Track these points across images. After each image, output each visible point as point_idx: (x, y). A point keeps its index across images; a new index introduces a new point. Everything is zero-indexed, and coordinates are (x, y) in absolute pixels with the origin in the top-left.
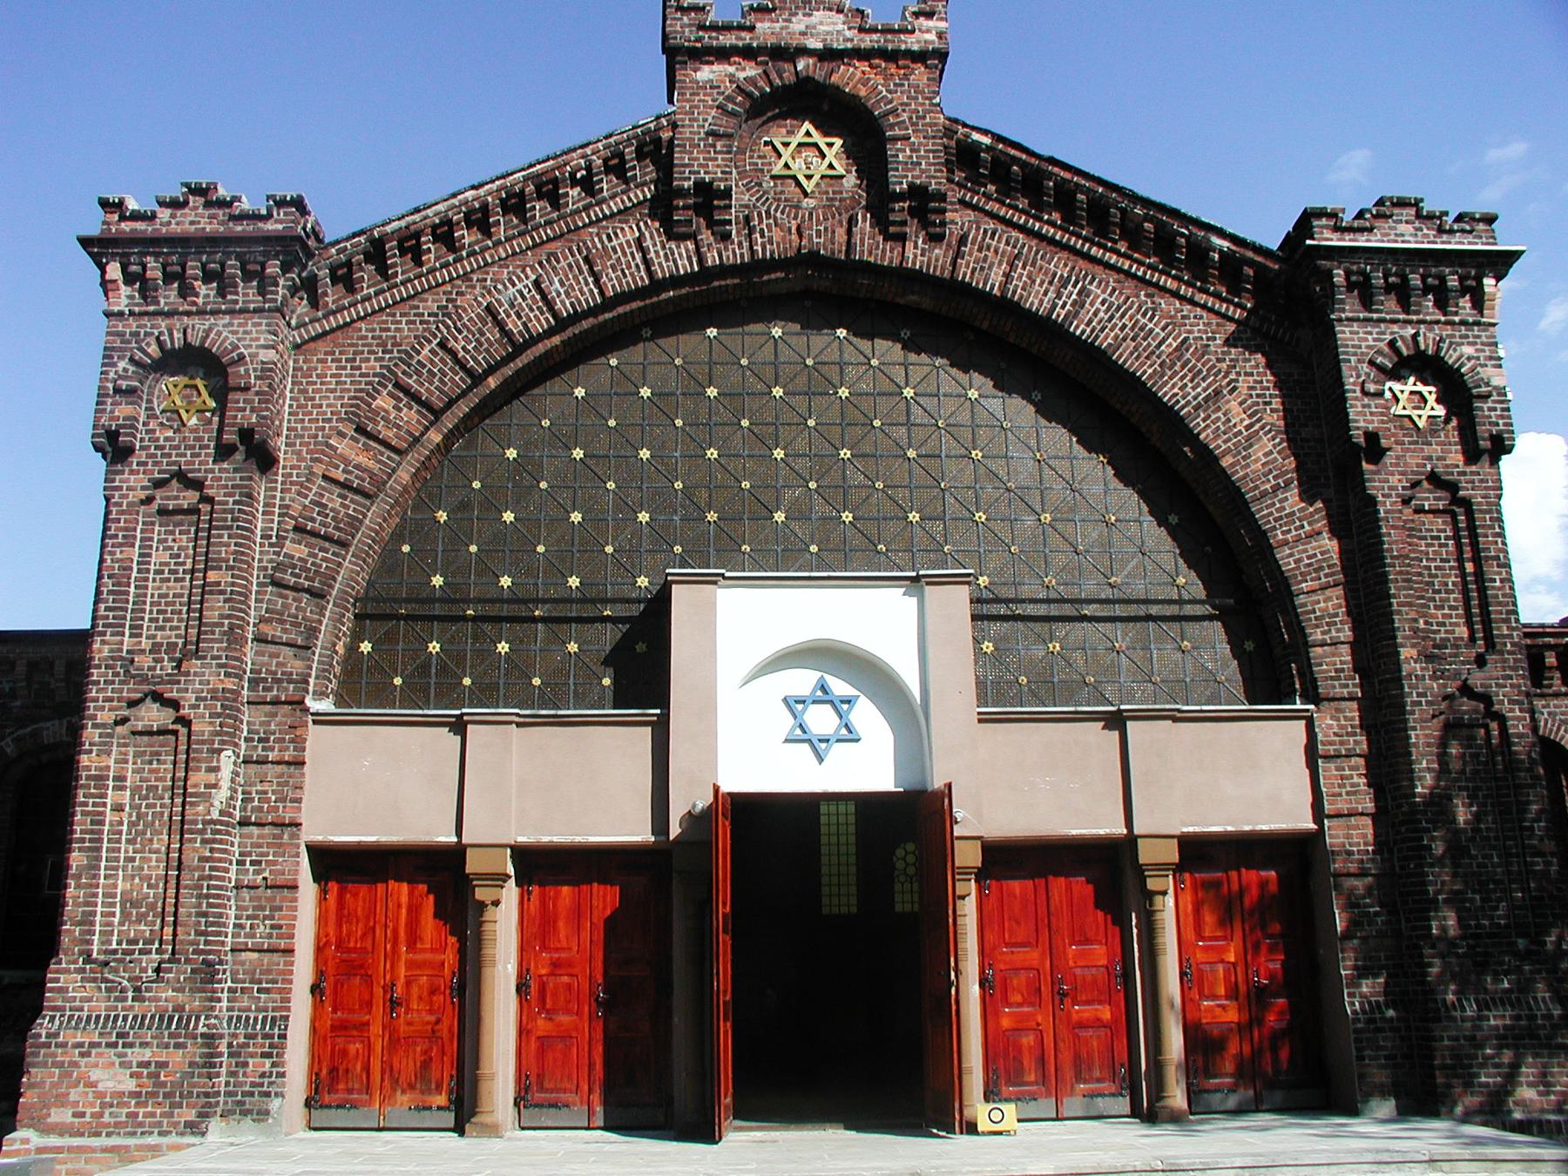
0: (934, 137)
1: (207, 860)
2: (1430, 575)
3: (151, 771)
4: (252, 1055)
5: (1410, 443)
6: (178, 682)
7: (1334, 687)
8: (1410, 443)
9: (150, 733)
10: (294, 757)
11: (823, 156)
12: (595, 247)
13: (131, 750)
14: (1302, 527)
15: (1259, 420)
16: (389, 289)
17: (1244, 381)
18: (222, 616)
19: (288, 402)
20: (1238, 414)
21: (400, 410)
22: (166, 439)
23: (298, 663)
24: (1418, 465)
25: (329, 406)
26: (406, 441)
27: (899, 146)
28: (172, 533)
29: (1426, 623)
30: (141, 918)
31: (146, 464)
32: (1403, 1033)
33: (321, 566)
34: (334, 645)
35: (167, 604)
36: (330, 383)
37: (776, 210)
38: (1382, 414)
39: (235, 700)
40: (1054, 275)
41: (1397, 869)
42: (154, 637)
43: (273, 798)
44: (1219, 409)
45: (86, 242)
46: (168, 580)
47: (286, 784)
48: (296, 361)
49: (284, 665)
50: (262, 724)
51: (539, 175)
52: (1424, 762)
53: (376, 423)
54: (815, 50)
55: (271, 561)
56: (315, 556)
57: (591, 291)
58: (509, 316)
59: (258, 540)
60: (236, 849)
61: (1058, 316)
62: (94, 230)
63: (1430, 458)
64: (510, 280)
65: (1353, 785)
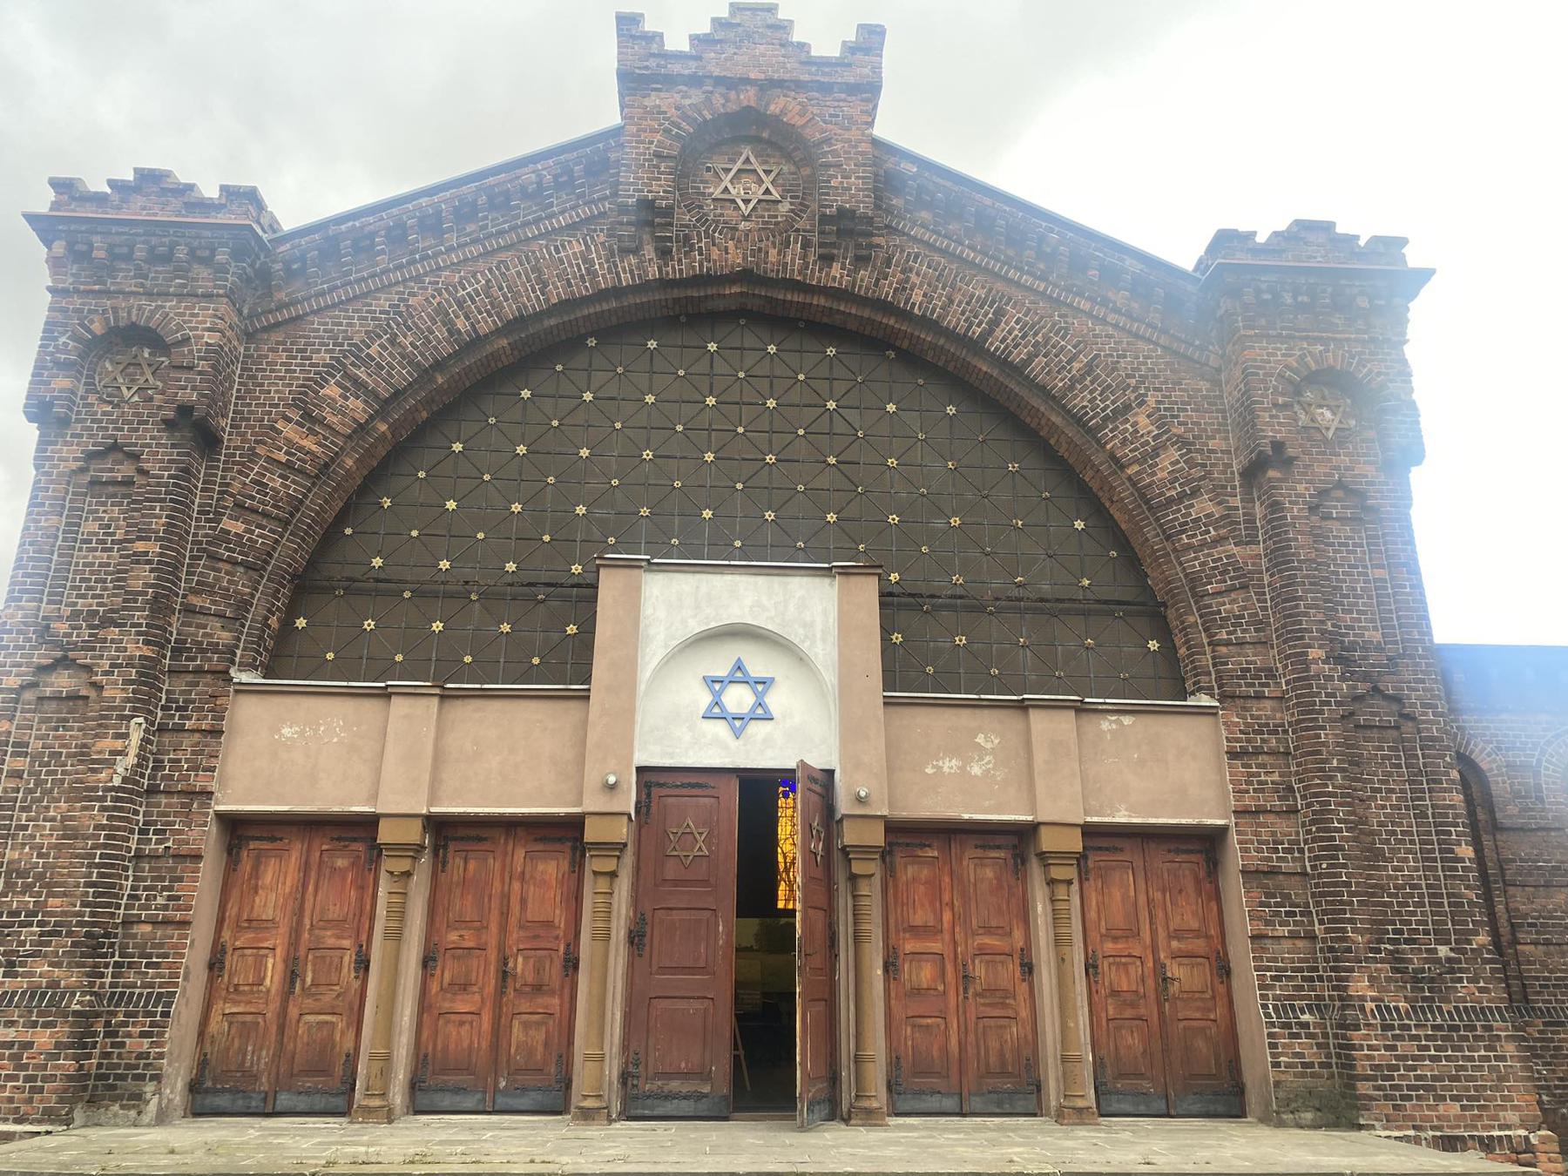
0: (864, 165)
1: (103, 828)
2: (1338, 580)
3: (56, 738)
4: (129, 1035)
5: (1318, 453)
6: (94, 649)
7: (1240, 686)
8: (1318, 453)
9: (60, 699)
10: (213, 725)
11: (760, 182)
12: (544, 259)
13: (37, 717)
14: (1208, 532)
15: (1165, 432)
16: (343, 286)
17: (1153, 396)
18: (146, 585)
19: (236, 386)
20: (1147, 426)
21: (346, 398)
22: (104, 413)
23: (225, 634)
24: (1325, 475)
25: (276, 392)
26: (350, 427)
27: (831, 172)
28: (104, 504)
29: (1333, 625)
30: (27, 888)
31: (81, 436)
32: (1321, 1040)
33: (257, 541)
34: (267, 618)
35: (92, 572)
36: (280, 371)
37: (714, 232)
38: (1289, 424)
39: (154, 668)
40: (972, 296)
41: (1309, 870)
42: (75, 604)
43: (186, 766)
44: (1127, 421)
45: (32, 219)
46: (95, 550)
47: (201, 752)
48: (246, 349)
49: (211, 636)
50: (182, 692)
51: (492, 187)
52: (1335, 761)
53: (321, 408)
54: (756, 80)
55: (206, 535)
56: (252, 532)
57: (537, 298)
58: (457, 317)
59: (195, 515)
60: (141, 817)
61: (974, 333)
62: (44, 209)
63: (1337, 468)
64: (460, 283)
65: (1260, 783)
